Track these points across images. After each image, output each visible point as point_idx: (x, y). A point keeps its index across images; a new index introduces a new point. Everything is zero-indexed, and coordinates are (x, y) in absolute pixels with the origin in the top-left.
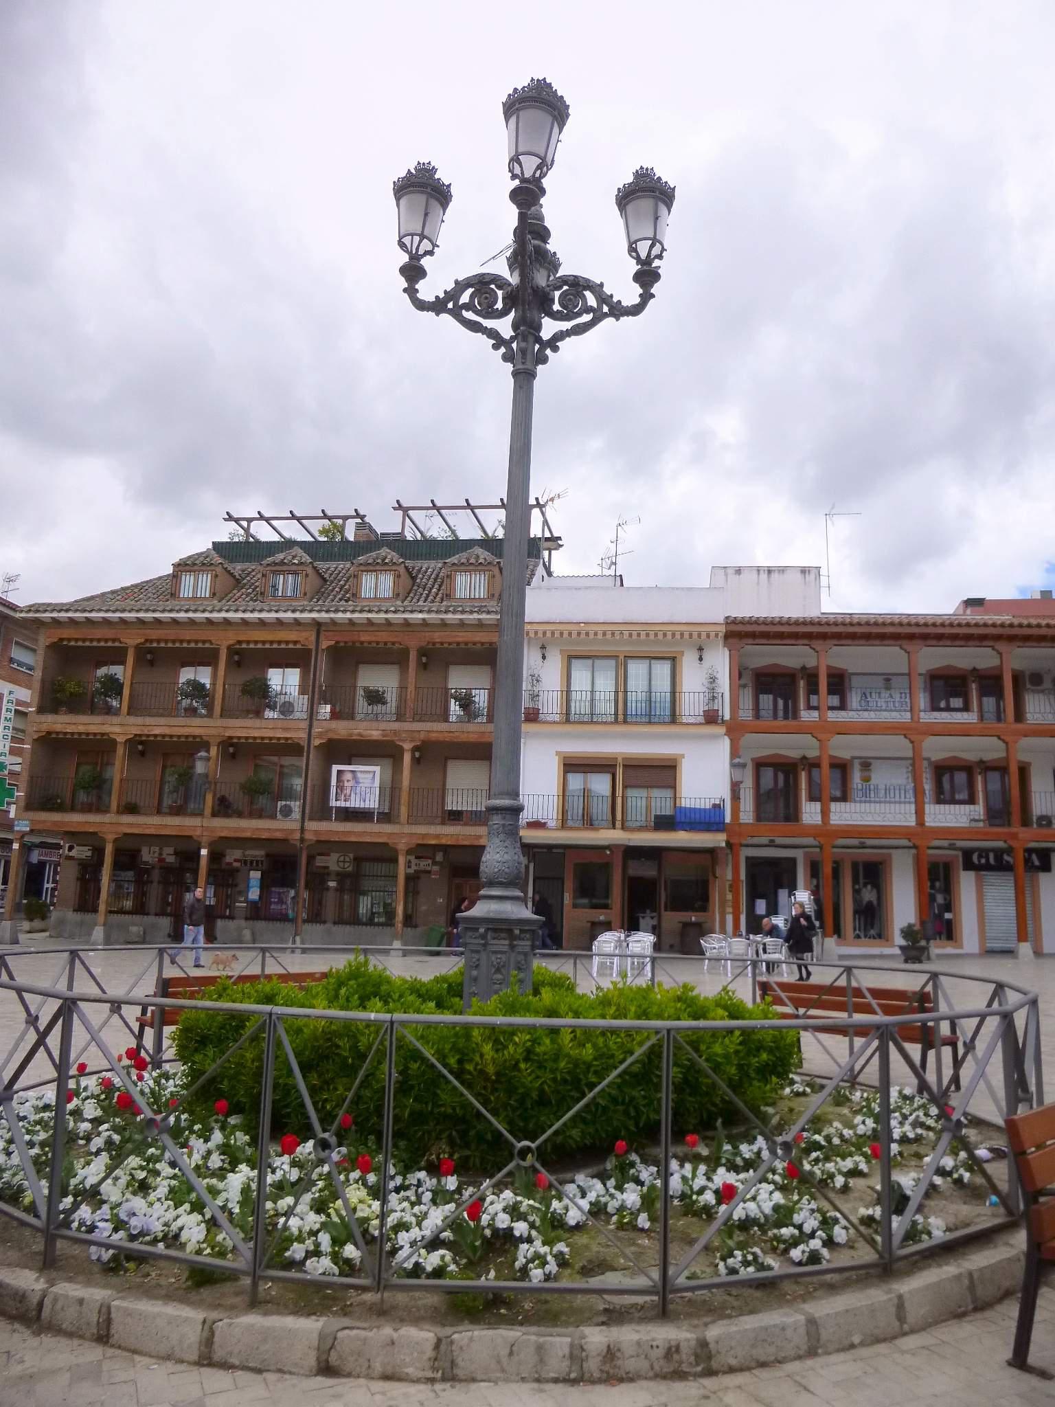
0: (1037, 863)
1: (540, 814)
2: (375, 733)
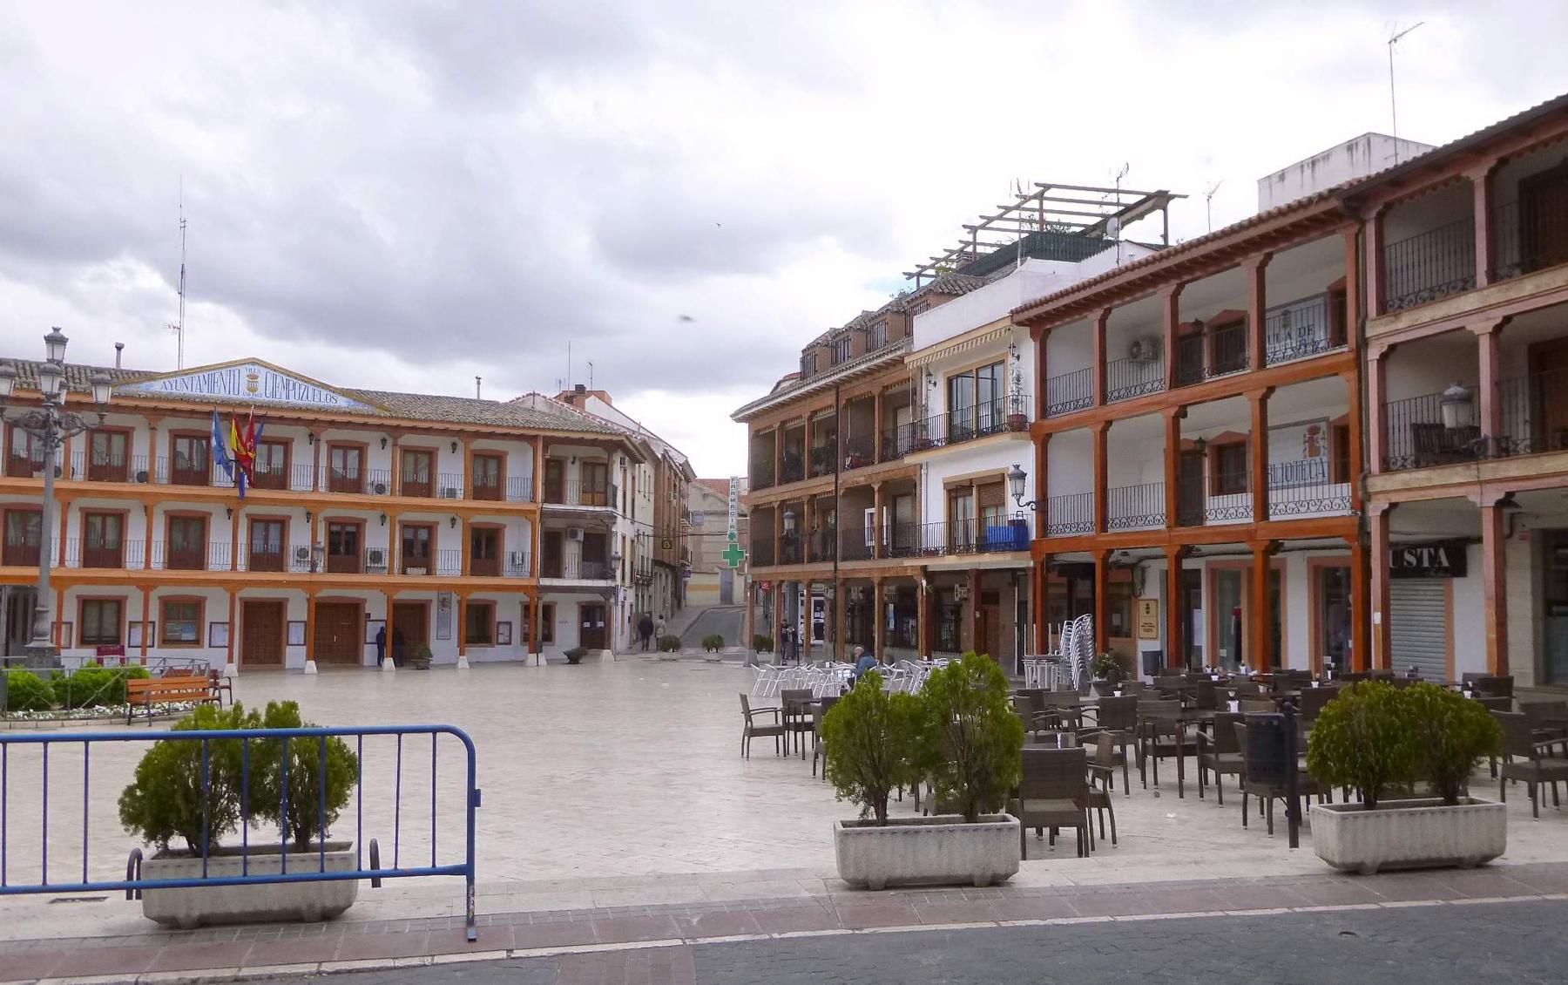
0: (1445, 563)
1: (1216, 500)
2: (862, 479)
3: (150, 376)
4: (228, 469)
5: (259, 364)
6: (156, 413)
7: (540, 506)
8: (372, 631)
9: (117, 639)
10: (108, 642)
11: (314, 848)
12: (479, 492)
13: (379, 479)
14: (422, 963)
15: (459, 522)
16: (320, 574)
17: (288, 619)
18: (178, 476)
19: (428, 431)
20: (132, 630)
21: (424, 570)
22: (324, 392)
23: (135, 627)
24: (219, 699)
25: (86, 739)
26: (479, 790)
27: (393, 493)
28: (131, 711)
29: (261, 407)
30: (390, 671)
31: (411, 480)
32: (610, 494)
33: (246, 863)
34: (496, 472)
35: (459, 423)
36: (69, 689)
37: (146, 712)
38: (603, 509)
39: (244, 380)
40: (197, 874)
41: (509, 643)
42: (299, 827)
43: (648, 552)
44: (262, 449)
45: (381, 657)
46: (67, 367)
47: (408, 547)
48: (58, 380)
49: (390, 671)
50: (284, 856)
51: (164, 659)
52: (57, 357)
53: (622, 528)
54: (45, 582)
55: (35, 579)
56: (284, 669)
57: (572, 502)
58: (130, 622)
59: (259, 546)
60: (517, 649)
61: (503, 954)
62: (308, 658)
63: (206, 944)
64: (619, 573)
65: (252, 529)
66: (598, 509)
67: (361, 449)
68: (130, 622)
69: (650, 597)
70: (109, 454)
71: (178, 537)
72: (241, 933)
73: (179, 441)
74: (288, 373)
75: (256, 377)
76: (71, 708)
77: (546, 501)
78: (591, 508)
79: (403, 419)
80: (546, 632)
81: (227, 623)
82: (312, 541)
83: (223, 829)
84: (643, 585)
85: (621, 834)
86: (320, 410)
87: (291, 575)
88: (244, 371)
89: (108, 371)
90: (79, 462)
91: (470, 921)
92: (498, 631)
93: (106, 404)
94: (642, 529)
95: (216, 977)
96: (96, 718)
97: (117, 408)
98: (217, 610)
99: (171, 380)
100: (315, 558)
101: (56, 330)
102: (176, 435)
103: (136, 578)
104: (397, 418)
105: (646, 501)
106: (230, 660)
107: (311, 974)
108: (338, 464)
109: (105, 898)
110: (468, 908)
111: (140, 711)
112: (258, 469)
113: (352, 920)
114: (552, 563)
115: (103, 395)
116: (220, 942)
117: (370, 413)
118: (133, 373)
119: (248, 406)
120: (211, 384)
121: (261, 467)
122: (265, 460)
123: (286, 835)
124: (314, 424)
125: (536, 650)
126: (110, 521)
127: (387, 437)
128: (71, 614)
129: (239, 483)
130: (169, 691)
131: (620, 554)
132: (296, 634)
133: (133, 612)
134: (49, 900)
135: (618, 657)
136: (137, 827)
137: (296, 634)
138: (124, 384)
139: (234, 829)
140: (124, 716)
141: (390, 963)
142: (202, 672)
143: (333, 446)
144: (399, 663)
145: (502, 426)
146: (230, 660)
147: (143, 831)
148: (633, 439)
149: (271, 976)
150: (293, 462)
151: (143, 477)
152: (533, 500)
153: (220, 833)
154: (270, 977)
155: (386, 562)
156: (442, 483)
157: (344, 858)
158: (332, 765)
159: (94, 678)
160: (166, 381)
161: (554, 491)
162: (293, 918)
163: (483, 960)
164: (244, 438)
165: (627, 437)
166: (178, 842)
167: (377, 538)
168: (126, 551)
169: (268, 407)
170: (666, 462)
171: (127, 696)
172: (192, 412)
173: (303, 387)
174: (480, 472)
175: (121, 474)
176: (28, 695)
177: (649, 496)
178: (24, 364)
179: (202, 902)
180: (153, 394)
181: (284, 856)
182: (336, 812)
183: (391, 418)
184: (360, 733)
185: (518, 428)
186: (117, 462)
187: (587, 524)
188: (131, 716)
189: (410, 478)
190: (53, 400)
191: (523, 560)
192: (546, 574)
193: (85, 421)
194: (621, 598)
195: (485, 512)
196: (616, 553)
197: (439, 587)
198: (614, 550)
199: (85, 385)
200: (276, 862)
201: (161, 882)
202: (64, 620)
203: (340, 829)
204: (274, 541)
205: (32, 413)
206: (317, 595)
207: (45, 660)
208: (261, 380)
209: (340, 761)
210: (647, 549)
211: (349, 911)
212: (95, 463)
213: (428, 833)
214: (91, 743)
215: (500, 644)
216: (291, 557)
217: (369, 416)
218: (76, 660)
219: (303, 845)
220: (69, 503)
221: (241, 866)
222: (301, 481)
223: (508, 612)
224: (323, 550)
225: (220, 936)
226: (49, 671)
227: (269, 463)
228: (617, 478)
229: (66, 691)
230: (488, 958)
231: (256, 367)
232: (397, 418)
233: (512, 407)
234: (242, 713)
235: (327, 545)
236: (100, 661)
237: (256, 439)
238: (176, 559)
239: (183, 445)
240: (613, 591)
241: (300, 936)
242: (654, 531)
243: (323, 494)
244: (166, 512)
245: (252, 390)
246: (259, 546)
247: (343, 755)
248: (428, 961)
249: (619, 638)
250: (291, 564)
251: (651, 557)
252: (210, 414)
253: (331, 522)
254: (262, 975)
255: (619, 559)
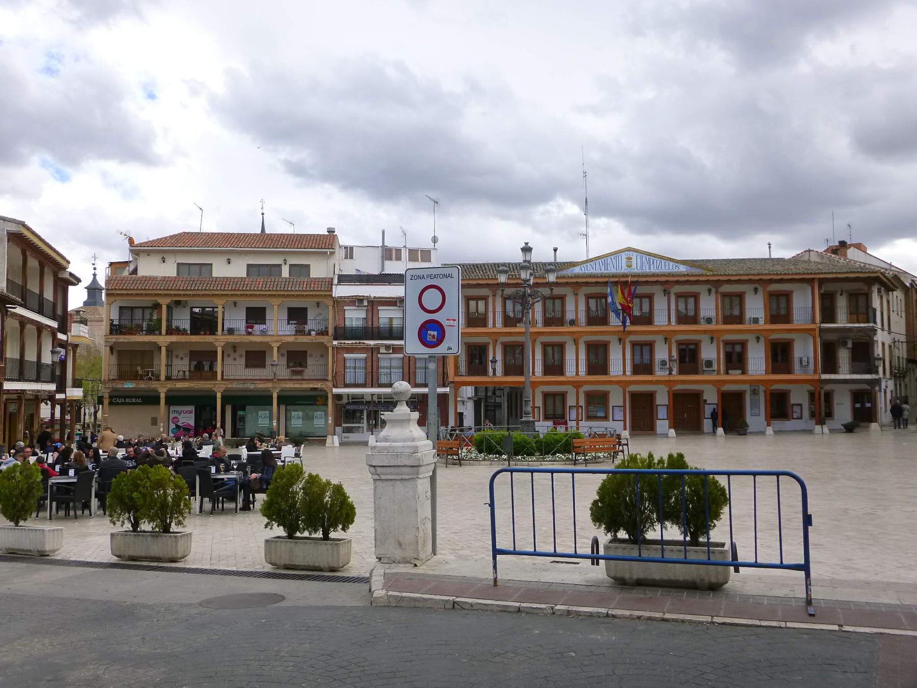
3: (573, 264)
4: (618, 315)
5: (632, 251)
6: (578, 285)
7: (818, 325)
8: (708, 410)
9: (563, 416)
10: (558, 418)
11: (703, 545)
12: (774, 318)
13: (708, 315)
14: (779, 626)
15: (762, 340)
16: (675, 376)
17: (657, 404)
18: (591, 321)
19: (739, 282)
20: (571, 411)
21: (740, 372)
22: (671, 264)
23: (572, 409)
24: (622, 451)
25: (552, 472)
26: (811, 515)
27: (717, 323)
28: (575, 458)
29: (634, 276)
30: (721, 436)
31: (729, 314)
32: (871, 314)
33: (663, 550)
34: (785, 305)
35: (759, 274)
36: (543, 444)
37: (583, 458)
38: (866, 325)
39: (624, 260)
40: (635, 554)
41: (801, 418)
42: (692, 530)
43: (903, 354)
44: (636, 301)
45: (715, 426)
46: (533, 264)
47: (729, 357)
48: (529, 272)
49: (721, 436)
50: (685, 548)
51: (591, 428)
52: (528, 259)
53: (881, 337)
54: (528, 385)
55: (523, 383)
56: (656, 434)
57: (842, 322)
58: (570, 407)
59: (638, 360)
60: (806, 422)
61: (836, 628)
62: (670, 427)
63: (642, 596)
64: (881, 369)
65: (633, 350)
66: (862, 325)
67: (696, 296)
68: (570, 407)
69: (906, 385)
70: (554, 311)
71: (592, 357)
72: (661, 592)
73: (590, 300)
74: (649, 254)
75: (631, 259)
76: (545, 455)
77: (823, 322)
78: (857, 325)
79: (721, 275)
80: (827, 411)
81: (622, 406)
82: (669, 355)
83: (648, 528)
84: (900, 377)
85: (907, 553)
86: (669, 275)
87: (659, 376)
88: (624, 256)
89: (550, 264)
90: (539, 317)
91: (809, 602)
92: (792, 410)
93: (553, 282)
94: (897, 337)
95: (651, 617)
96: (558, 461)
97: (557, 284)
98: (616, 399)
99: (584, 265)
100: (671, 365)
101: (527, 244)
102: (588, 297)
103: (571, 381)
104: (718, 275)
105: (897, 316)
106: (625, 429)
107: (708, 623)
108: (682, 307)
109: (578, 563)
110: (807, 593)
111: (580, 458)
112: (635, 314)
113: (728, 592)
114: (830, 364)
115: (552, 278)
116: (650, 596)
117: (701, 273)
118: (564, 263)
119: (627, 276)
120: (606, 265)
121: (636, 313)
122: (638, 308)
123: (685, 536)
124: (666, 283)
125: (821, 422)
126: (556, 348)
127: (711, 287)
128: (539, 402)
129: (624, 322)
130: (595, 446)
131: (881, 356)
132: (662, 413)
133: (571, 401)
134: (552, 560)
135: (883, 428)
136: (600, 524)
137: (662, 413)
138: (559, 271)
139: (654, 529)
140: (572, 460)
141: (757, 623)
142: (612, 436)
143: (679, 296)
144: (727, 431)
145: (788, 274)
146: (625, 429)
147: (604, 526)
148: (887, 275)
149: (683, 620)
150: (701, 307)
151: (573, 323)
152: (813, 322)
153: (646, 531)
154: (683, 621)
155: (715, 367)
156: (749, 314)
157: (722, 552)
158: (711, 493)
159: (555, 438)
160: (581, 266)
161: (829, 314)
162: (692, 587)
163: (822, 630)
164: (626, 295)
165: (881, 273)
166: (622, 534)
167: (708, 352)
168: (565, 363)
169: (639, 276)
170: (913, 289)
171: (573, 449)
172: (597, 283)
173: (659, 261)
174: (774, 306)
175: (560, 321)
176: (524, 447)
177: (901, 314)
178: (509, 265)
179: (638, 571)
180: (575, 275)
181: (685, 548)
182: (714, 523)
183: (714, 275)
184: (729, 474)
185: (800, 274)
186: (558, 315)
187: (855, 336)
188: (576, 460)
189: (727, 313)
190: (527, 283)
191: (808, 362)
192: (825, 371)
193: (543, 293)
194: (883, 387)
195: (779, 331)
196: (878, 355)
197: (751, 382)
198: (876, 353)
199: (540, 273)
200: (680, 551)
201: (616, 557)
202: (536, 406)
203: (718, 533)
204: (646, 357)
205: (517, 290)
206: (674, 389)
207: (530, 428)
208: (634, 261)
209: (715, 491)
210: (902, 352)
211: (726, 586)
212: (547, 316)
213: (801, 540)
214: (554, 474)
215: (795, 419)
216: (657, 366)
217: (699, 275)
218: (544, 427)
219: (695, 542)
220: (535, 340)
221: (660, 552)
222: (661, 319)
223: (799, 397)
224: (675, 360)
225: (650, 593)
226: (532, 434)
227: (641, 309)
228: (876, 303)
229: (542, 446)
230: (825, 628)
231: (631, 253)
232: (718, 275)
233: (795, 260)
234: (653, 459)
235: (678, 357)
236: (556, 428)
237: (633, 296)
238: (592, 369)
239: (592, 303)
240: (877, 382)
241: (696, 599)
242: (907, 339)
243: (674, 326)
244: (585, 342)
245: (629, 266)
246: (638, 360)
247: (717, 487)
248: (783, 624)
249: (883, 415)
250: (657, 370)
251: (905, 356)
252: (606, 283)
253: (679, 343)
254: (678, 619)
255: (880, 359)
